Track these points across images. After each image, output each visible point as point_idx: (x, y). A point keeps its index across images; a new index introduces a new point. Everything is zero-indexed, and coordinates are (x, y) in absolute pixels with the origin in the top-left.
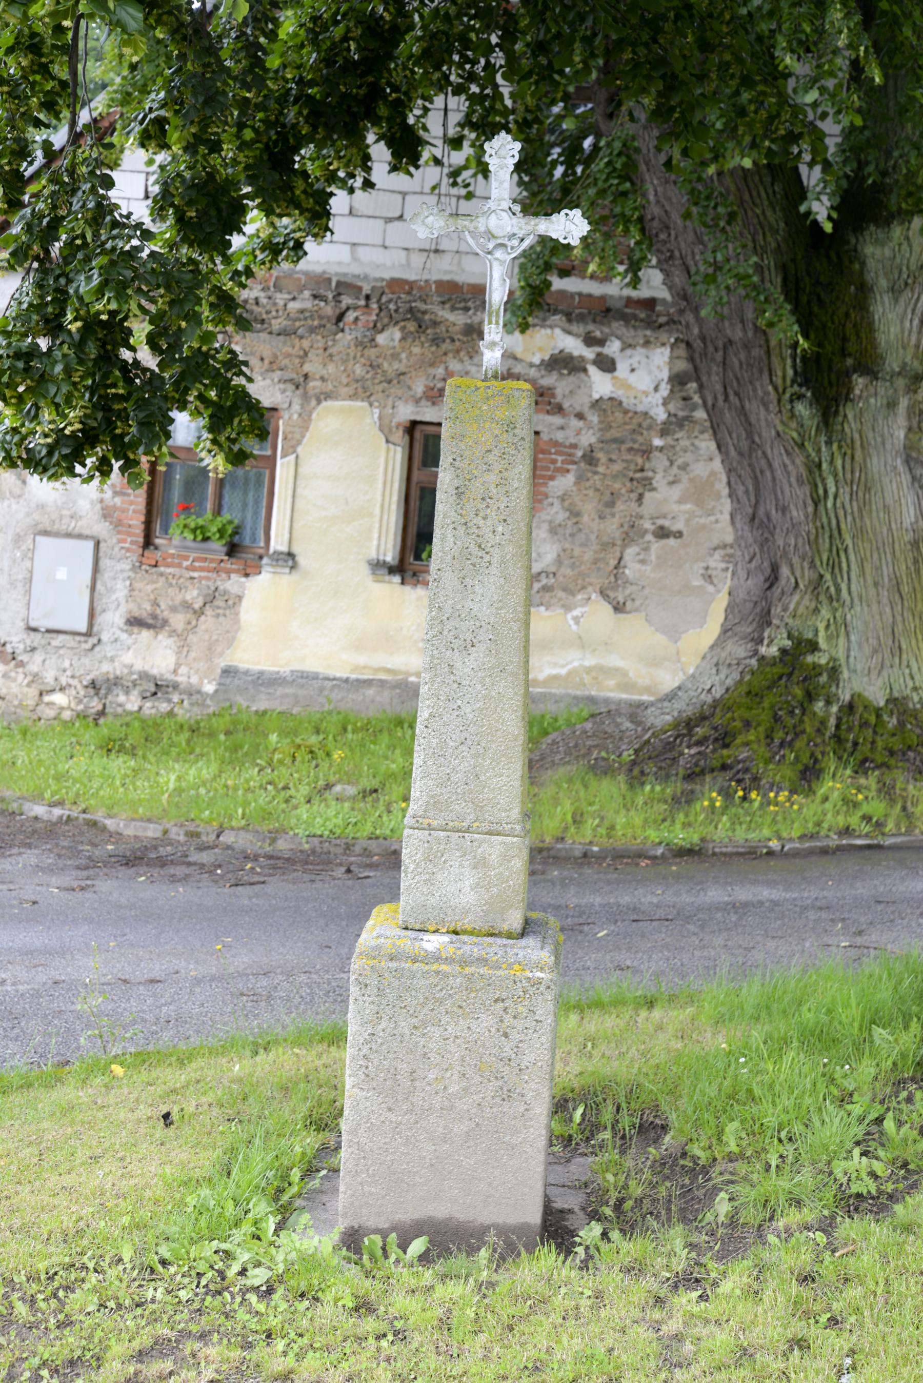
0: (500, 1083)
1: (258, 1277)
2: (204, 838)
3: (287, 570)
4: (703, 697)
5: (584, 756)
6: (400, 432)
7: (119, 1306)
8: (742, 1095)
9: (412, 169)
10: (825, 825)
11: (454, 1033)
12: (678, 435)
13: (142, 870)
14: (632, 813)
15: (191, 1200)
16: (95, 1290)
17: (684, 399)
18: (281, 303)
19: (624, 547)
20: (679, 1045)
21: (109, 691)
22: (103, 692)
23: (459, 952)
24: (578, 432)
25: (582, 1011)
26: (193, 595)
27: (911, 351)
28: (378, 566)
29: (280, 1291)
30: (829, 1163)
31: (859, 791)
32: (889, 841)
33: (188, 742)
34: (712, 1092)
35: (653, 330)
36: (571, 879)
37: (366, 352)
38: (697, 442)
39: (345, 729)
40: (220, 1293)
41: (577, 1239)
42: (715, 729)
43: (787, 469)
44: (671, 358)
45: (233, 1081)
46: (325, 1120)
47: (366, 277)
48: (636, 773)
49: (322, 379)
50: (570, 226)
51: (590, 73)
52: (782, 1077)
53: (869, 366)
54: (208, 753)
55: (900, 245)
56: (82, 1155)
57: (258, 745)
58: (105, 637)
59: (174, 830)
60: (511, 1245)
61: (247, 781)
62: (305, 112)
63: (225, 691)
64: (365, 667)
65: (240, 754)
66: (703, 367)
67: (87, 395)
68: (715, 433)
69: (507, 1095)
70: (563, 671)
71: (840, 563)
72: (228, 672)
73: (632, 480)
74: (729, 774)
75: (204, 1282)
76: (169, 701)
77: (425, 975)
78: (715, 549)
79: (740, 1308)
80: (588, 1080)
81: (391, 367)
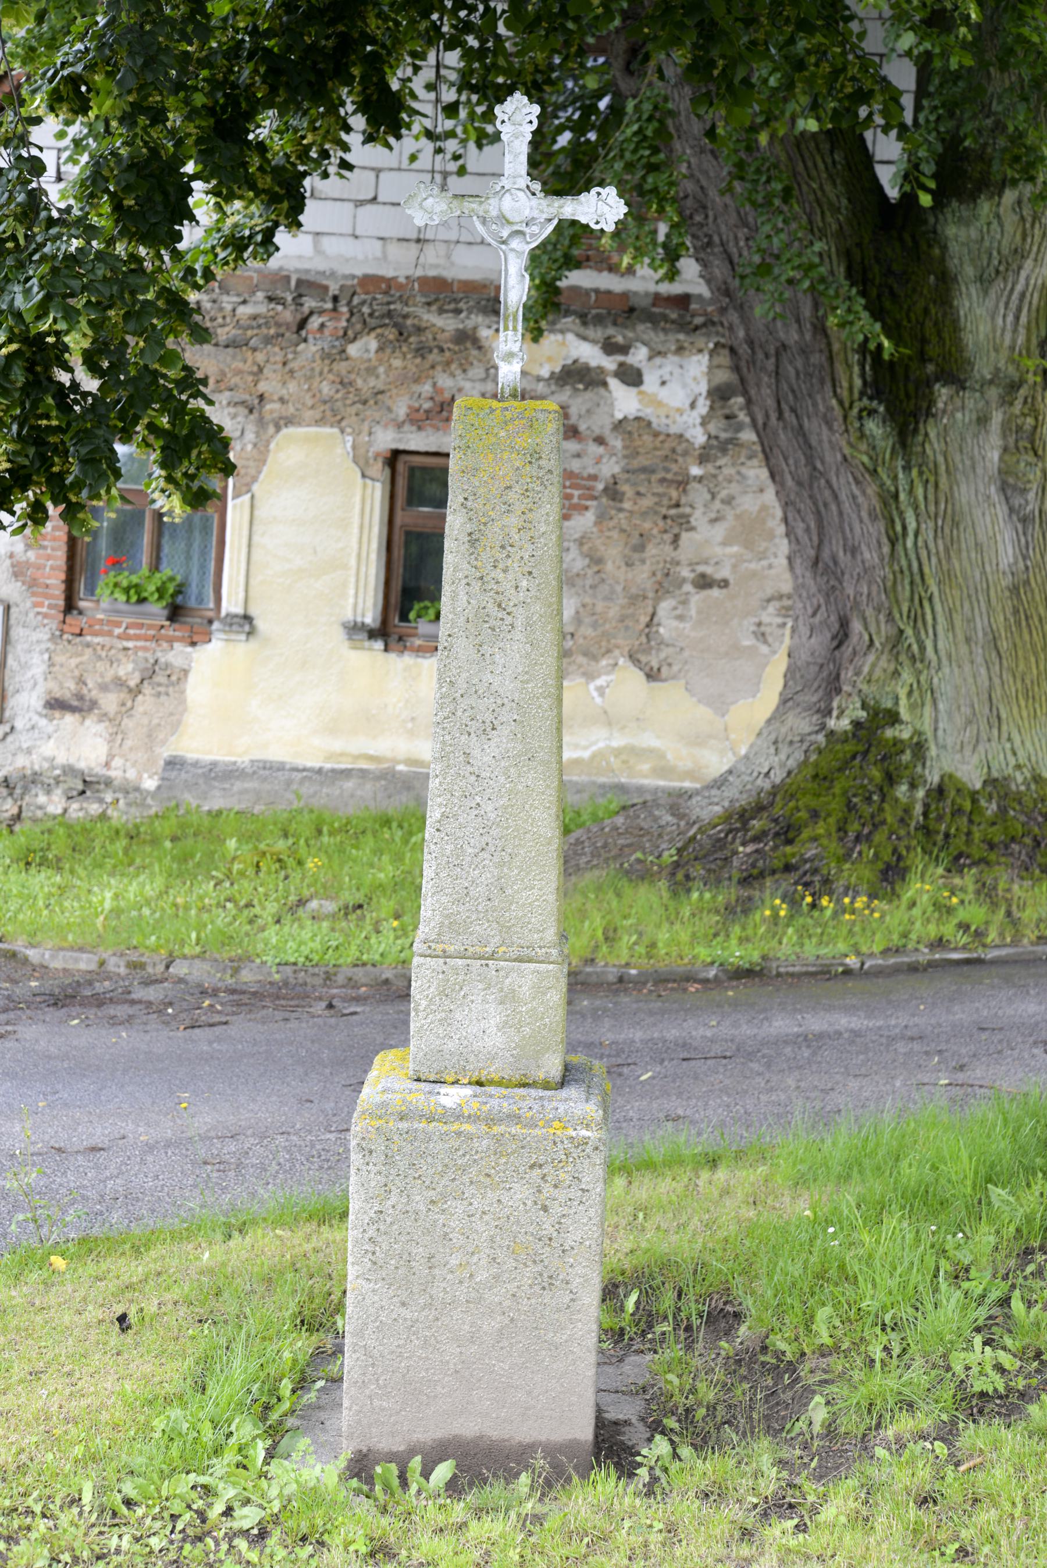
0: (539, 1268)
1: (248, 1518)
2: (150, 970)
3: (243, 637)
4: (759, 782)
5: (615, 858)
6: (379, 464)
7: (76, 1559)
8: (833, 1273)
9: (392, 140)
10: (913, 936)
11: (479, 1205)
12: (720, 462)
13: (75, 1010)
14: (677, 926)
15: (159, 1424)
16: (44, 1540)
17: (728, 417)
18: (229, 307)
19: (657, 600)
20: (752, 1213)
21: (26, 790)
22: (18, 791)
23: (485, 1108)
24: (598, 461)
25: (630, 1174)
26: (127, 670)
27: (1004, 354)
28: (354, 629)
29: (276, 1533)
30: (945, 1356)
31: (953, 893)
32: (991, 954)
33: (126, 851)
34: (796, 1270)
35: (687, 333)
36: (605, 1010)
37: (335, 366)
38: (744, 470)
39: (320, 832)
40: (200, 1539)
41: (639, 1459)
42: (776, 821)
43: (856, 501)
44: (710, 368)
45: (202, 1273)
46: (320, 1318)
47: (333, 274)
48: (679, 876)
49: (282, 400)
50: (602, 208)
51: (613, 19)
52: (881, 1250)
53: (955, 373)
54: (151, 864)
55: (989, 224)
56: (18, 1371)
57: (213, 853)
58: (19, 724)
59: (113, 960)
60: (559, 1470)
61: (201, 898)
62: (262, 70)
63: (170, 788)
64: (342, 755)
65: (191, 864)
66: (751, 378)
67: (15, 427)
68: (767, 458)
69: (548, 1283)
70: (586, 754)
71: (923, 615)
72: (173, 763)
73: (665, 517)
74: (793, 877)
75: (180, 1526)
76: (101, 801)
77: (443, 1136)
78: (769, 601)
79: (847, 1539)
80: (640, 1259)
81: (365, 385)
